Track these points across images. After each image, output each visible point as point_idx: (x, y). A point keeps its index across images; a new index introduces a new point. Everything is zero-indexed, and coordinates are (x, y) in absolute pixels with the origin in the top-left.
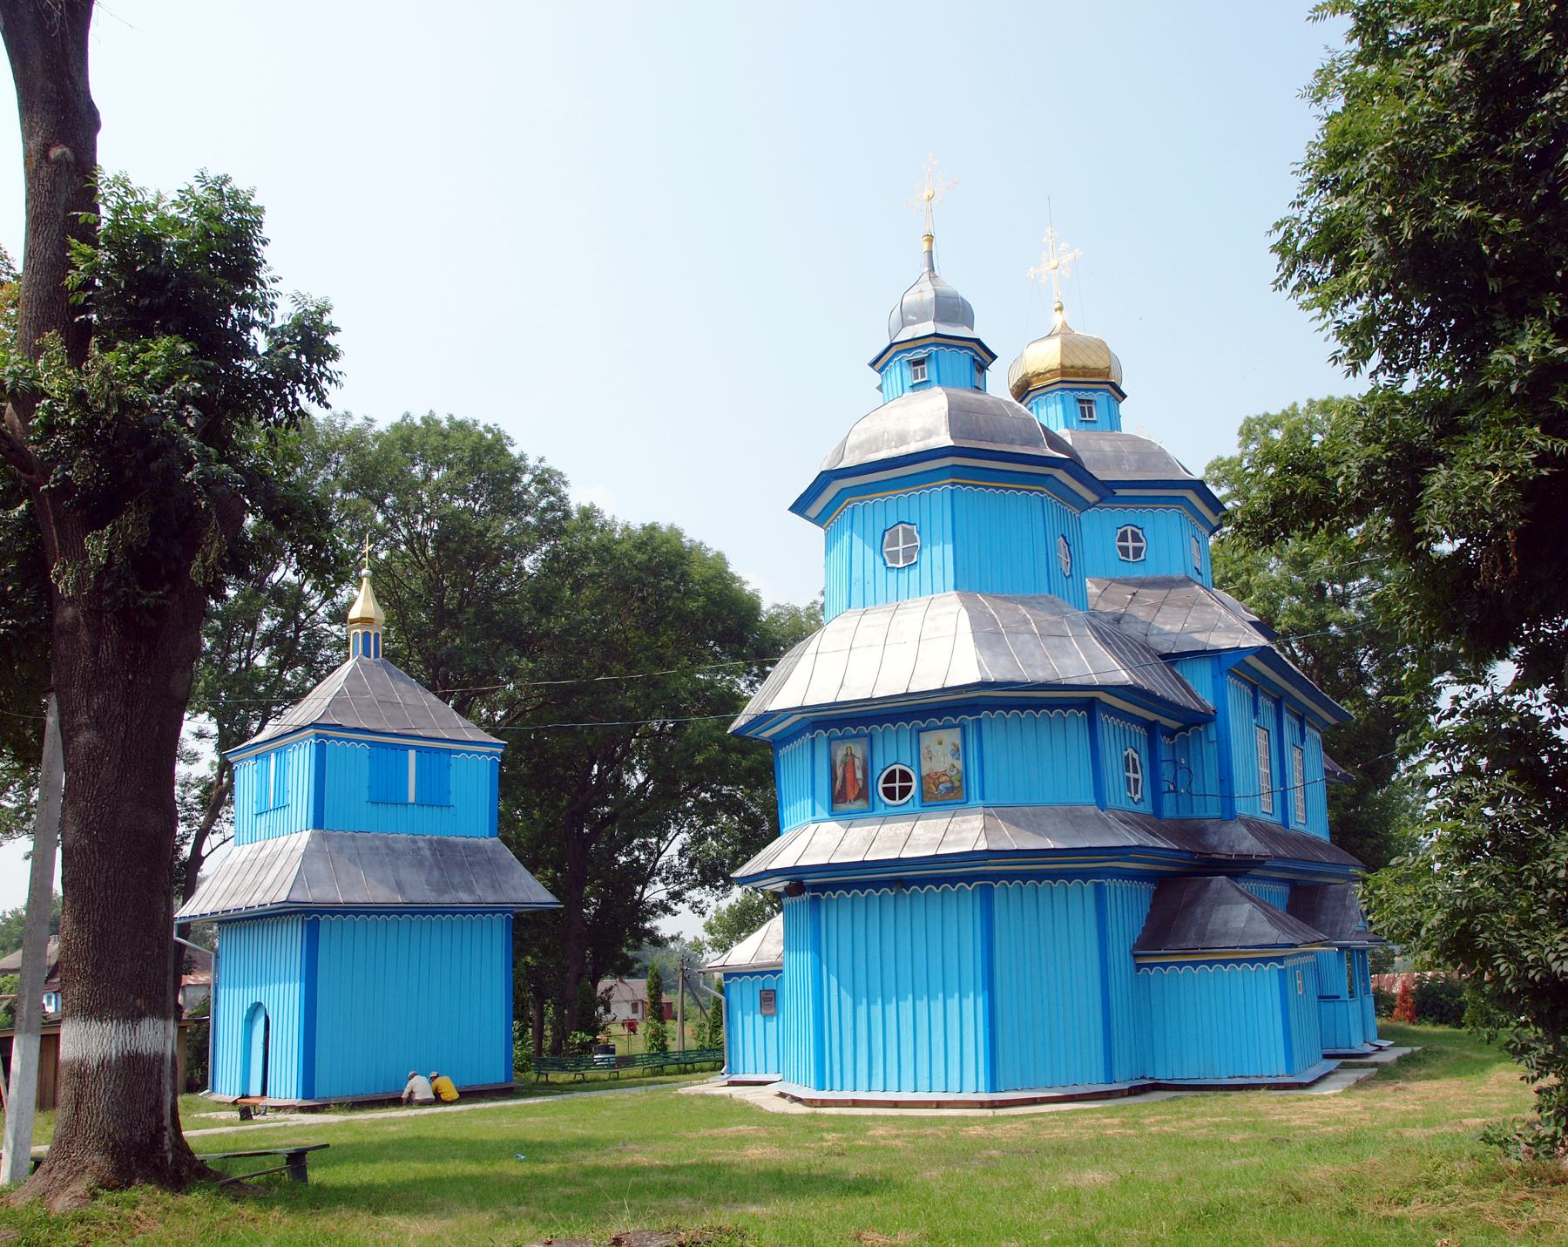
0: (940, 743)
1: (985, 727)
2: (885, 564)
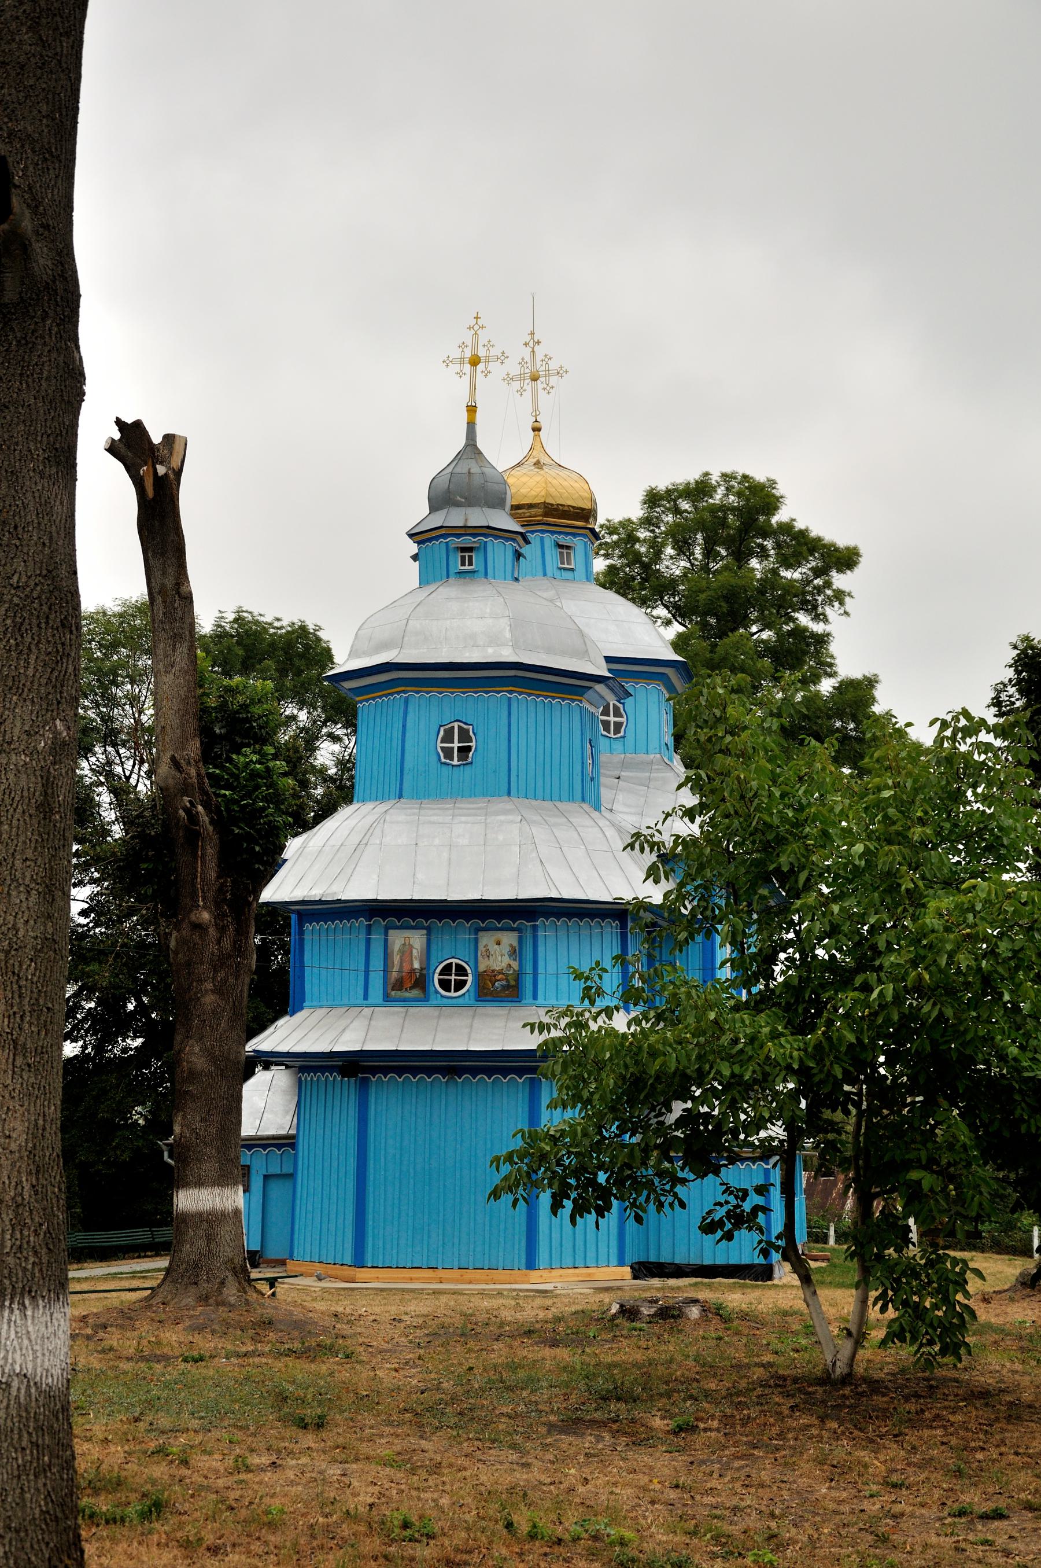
0: (498, 943)
1: (541, 933)
2: (440, 759)
